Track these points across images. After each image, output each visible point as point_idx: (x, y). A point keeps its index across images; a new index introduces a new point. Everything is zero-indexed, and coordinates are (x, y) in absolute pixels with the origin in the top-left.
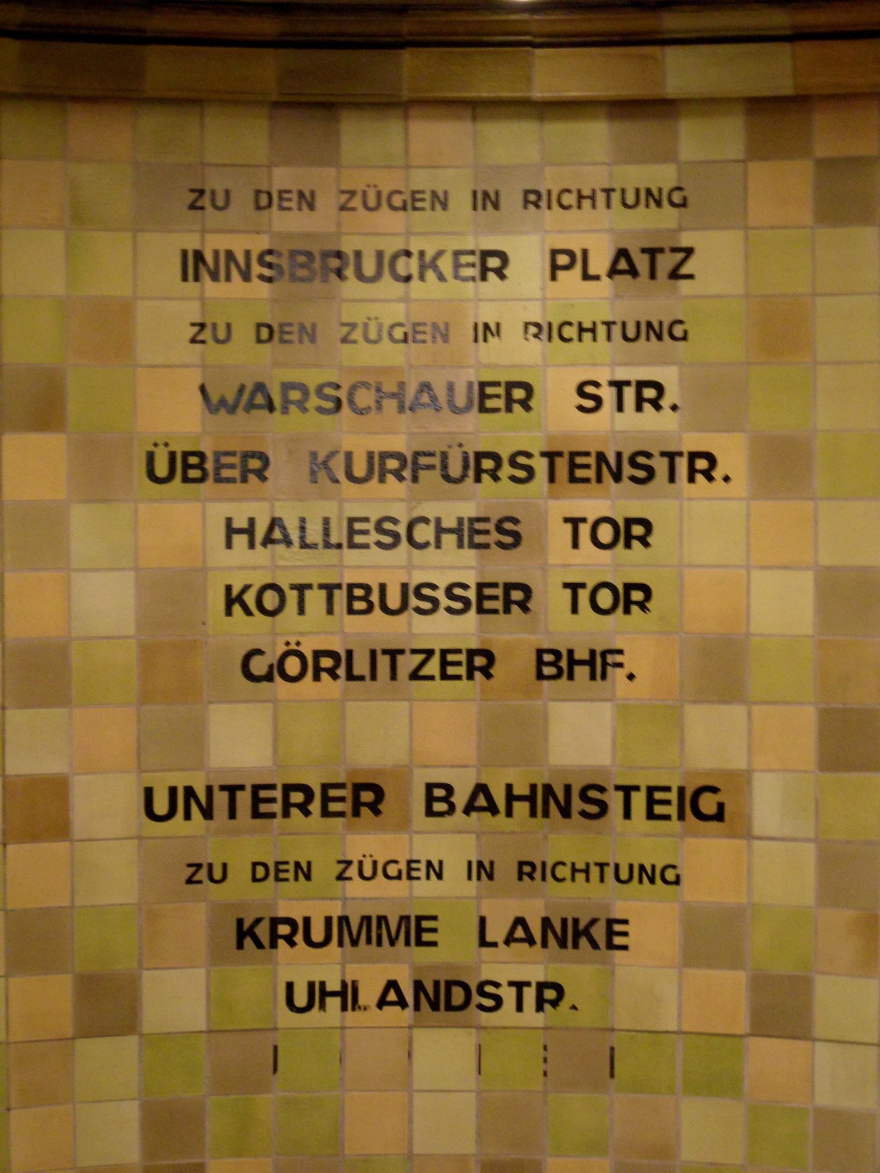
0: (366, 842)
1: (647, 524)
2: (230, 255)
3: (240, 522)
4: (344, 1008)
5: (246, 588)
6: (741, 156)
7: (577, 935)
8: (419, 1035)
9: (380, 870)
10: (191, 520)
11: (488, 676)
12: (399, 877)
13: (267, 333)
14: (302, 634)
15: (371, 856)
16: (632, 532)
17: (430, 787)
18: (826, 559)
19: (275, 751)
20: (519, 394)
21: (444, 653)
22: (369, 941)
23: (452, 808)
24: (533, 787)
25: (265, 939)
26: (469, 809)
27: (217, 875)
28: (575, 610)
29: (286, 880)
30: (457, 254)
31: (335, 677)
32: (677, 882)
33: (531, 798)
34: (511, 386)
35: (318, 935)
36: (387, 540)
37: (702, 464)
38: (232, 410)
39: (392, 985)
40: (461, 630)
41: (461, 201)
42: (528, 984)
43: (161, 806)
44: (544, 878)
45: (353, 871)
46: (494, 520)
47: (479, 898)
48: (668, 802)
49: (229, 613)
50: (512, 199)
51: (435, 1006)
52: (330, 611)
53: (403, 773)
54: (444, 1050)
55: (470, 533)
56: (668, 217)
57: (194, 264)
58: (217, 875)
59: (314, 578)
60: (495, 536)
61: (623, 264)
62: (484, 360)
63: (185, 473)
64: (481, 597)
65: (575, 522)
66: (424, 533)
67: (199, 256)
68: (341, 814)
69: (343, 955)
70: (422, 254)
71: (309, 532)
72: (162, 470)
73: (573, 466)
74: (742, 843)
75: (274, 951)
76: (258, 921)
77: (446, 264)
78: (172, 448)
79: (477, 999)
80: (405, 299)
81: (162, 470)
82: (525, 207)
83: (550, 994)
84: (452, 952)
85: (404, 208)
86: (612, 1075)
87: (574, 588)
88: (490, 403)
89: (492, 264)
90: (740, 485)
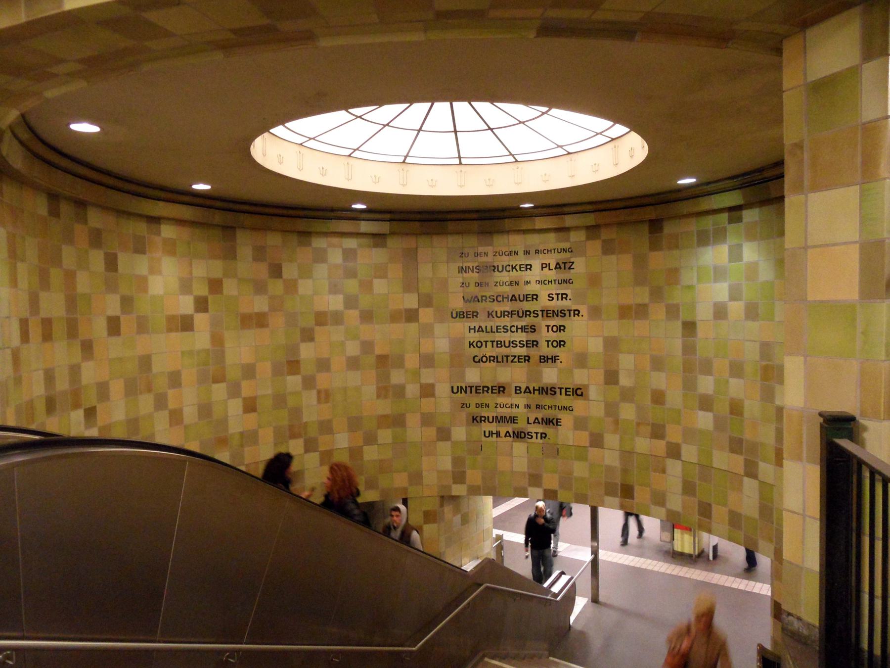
0: (501, 400)
8: (514, 444)
9: (505, 406)
10: (461, 327)
13: (478, 284)
16: (561, 328)
18: (606, 335)
33: (539, 390)
35: (491, 420)
37: (577, 313)
40: (523, 351)
41: (521, 253)
43: (455, 390)
53: (509, 384)
54: (519, 448)
55: (524, 329)
56: (568, 255)
61: (558, 266)
65: (548, 326)
72: (454, 315)
73: (547, 313)
74: (586, 402)
77: (518, 268)
84: (521, 425)
87: (548, 341)
89: (529, 267)
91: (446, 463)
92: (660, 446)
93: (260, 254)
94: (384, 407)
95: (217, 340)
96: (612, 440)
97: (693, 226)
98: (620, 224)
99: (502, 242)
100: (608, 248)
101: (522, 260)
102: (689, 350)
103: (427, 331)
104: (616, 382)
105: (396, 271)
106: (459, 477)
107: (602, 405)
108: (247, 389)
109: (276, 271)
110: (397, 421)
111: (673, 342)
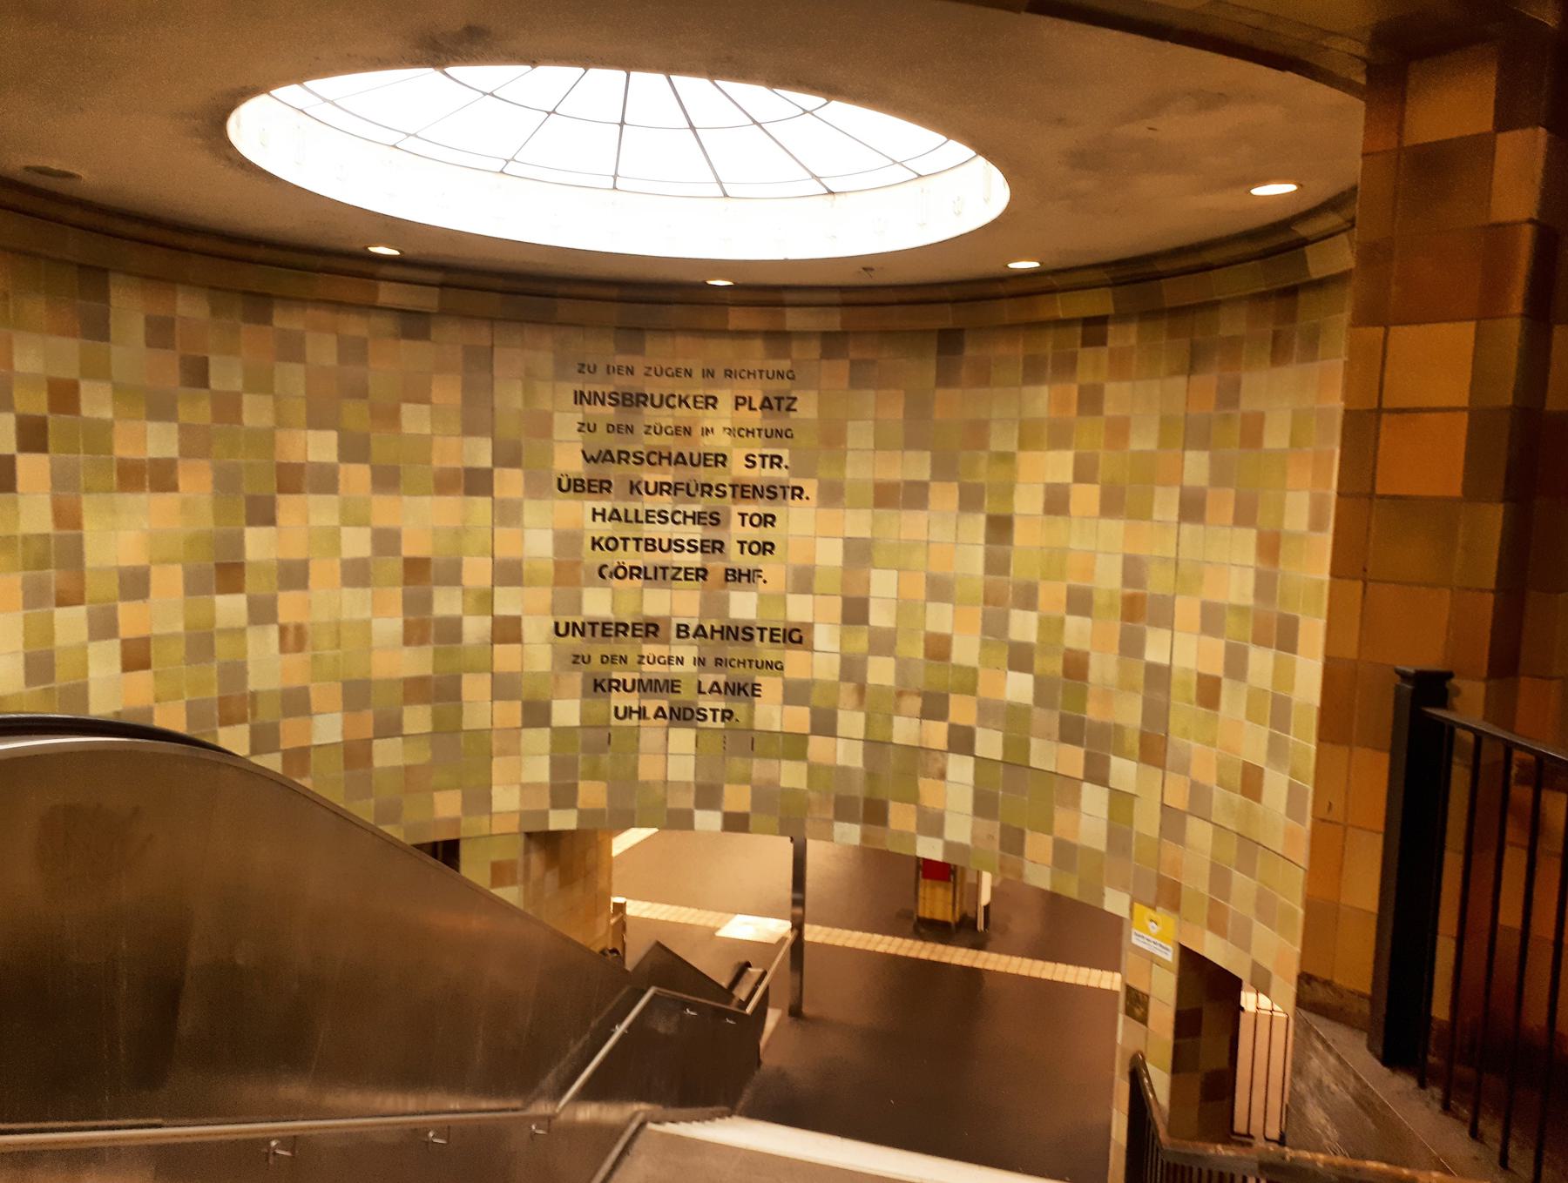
0: (650, 649)
1: (773, 517)
3: (599, 510)
9: (657, 660)
10: (580, 512)
13: (611, 428)
26: (695, 635)
34: (717, 455)
35: (629, 686)
37: (798, 492)
38: (596, 461)
40: (695, 560)
41: (697, 373)
43: (562, 630)
50: (719, 373)
53: (668, 620)
54: (683, 738)
55: (697, 518)
57: (580, 398)
59: (630, 535)
61: (766, 404)
65: (743, 515)
66: (679, 518)
67: (582, 394)
72: (564, 486)
73: (743, 491)
77: (690, 402)
80: (673, 416)
81: (564, 486)
84: (686, 695)
87: (742, 543)
89: (711, 402)
90: (813, 498)
91: (539, 770)
92: (936, 734)
93: (160, 332)
94: (418, 662)
95: (67, 517)
96: (852, 722)
97: (1010, 351)
98: (886, 333)
99: (659, 351)
100: (859, 379)
101: (697, 387)
102: (996, 565)
103: (508, 514)
104: (864, 620)
105: (448, 392)
106: (563, 795)
107: (837, 659)
108: (132, 619)
109: (197, 374)
110: (440, 691)
111: (968, 555)
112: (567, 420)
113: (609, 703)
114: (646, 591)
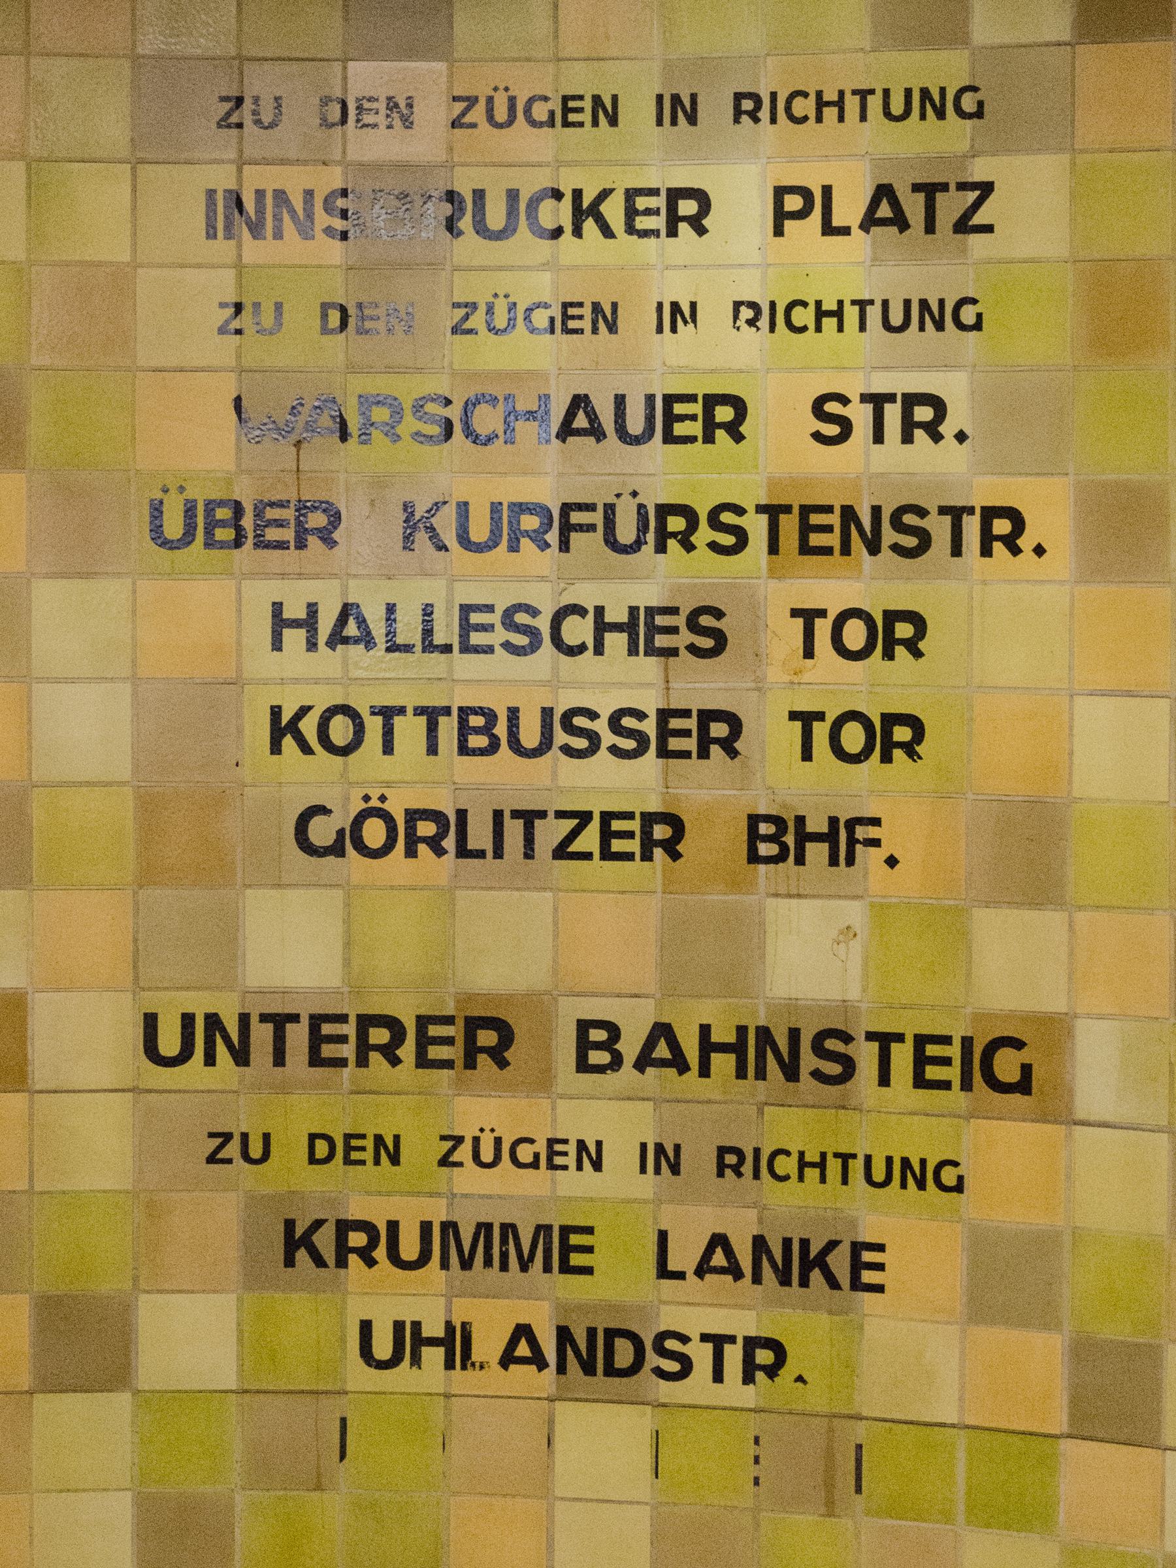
0: (484, 1108)
1: (917, 620)
2: (281, 196)
3: (295, 610)
4: (449, 1365)
5: (304, 711)
6: (1066, 37)
7: (807, 1266)
11: (675, 856)
12: (535, 1165)
14: (388, 784)
15: (492, 1130)
16: (895, 633)
17: (584, 1026)
19: (347, 962)
20: (724, 414)
21: (607, 817)
22: (488, 1262)
23: (617, 1061)
24: (742, 1030)
25: (329, 1255)
26: (642, 1064)
27: (256, 1151)
28: (807, 755)
29: (362, 1163)
30: (631, 195)
31: (440, 852)
32: (959, 1188)
33: (738, 1048)
35: (409, 1249)
36: (522, 640)
37: (1003, 528)
39: (523, 1331)
40: (627, 783)
41: (638, 111)
42: (732, 1339)
44: (756, 1175)
45: (464, 1153)
46: (684, 613)
47: (658, 1201)
48: (946, 1061)
49: (276, 748)
51: (588, 1368)
52: (432, 749)
53: (539, 1003)
54: (602, 1437)
55: (643, 630)
56: (949, 137)
58: (256, 1151)
60: (686, 637)
61: (885, 209)
62: (673, 361)
63: (209, 532)
64: (664, 733)
65: (808, 616)
68: (448, 1064)
69: (449, 1284)
70: (578, 194)
71: (399, 626)
72: (173, 527)
73: (809, 527)
75: (342, 1271)
76: (318, 1224)
78: (190, 494)
79: (652, 1359)
82: (737, 120)
83: (764, 1357)
84: (617, 1284)
85: (551, 123)
86: (859, 1490)
87: (806, 719)
88: (679, 429)
89: (686, 210)
90: (1062, 558)
112: (187, 288)
113: (342, 1313)
114: (463, 898)
